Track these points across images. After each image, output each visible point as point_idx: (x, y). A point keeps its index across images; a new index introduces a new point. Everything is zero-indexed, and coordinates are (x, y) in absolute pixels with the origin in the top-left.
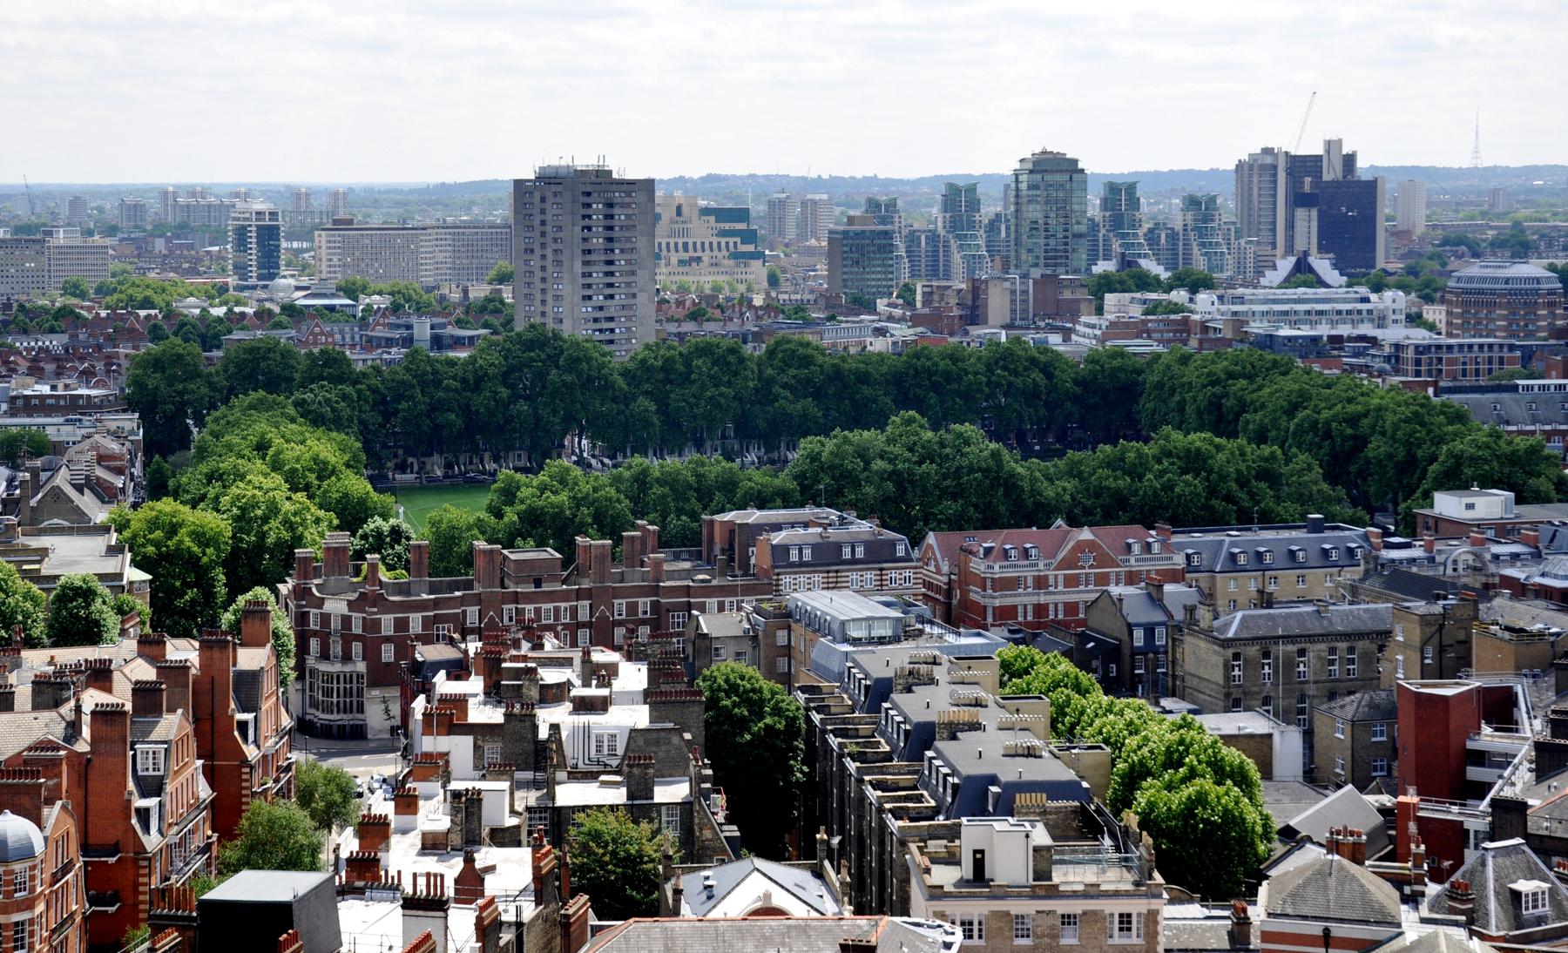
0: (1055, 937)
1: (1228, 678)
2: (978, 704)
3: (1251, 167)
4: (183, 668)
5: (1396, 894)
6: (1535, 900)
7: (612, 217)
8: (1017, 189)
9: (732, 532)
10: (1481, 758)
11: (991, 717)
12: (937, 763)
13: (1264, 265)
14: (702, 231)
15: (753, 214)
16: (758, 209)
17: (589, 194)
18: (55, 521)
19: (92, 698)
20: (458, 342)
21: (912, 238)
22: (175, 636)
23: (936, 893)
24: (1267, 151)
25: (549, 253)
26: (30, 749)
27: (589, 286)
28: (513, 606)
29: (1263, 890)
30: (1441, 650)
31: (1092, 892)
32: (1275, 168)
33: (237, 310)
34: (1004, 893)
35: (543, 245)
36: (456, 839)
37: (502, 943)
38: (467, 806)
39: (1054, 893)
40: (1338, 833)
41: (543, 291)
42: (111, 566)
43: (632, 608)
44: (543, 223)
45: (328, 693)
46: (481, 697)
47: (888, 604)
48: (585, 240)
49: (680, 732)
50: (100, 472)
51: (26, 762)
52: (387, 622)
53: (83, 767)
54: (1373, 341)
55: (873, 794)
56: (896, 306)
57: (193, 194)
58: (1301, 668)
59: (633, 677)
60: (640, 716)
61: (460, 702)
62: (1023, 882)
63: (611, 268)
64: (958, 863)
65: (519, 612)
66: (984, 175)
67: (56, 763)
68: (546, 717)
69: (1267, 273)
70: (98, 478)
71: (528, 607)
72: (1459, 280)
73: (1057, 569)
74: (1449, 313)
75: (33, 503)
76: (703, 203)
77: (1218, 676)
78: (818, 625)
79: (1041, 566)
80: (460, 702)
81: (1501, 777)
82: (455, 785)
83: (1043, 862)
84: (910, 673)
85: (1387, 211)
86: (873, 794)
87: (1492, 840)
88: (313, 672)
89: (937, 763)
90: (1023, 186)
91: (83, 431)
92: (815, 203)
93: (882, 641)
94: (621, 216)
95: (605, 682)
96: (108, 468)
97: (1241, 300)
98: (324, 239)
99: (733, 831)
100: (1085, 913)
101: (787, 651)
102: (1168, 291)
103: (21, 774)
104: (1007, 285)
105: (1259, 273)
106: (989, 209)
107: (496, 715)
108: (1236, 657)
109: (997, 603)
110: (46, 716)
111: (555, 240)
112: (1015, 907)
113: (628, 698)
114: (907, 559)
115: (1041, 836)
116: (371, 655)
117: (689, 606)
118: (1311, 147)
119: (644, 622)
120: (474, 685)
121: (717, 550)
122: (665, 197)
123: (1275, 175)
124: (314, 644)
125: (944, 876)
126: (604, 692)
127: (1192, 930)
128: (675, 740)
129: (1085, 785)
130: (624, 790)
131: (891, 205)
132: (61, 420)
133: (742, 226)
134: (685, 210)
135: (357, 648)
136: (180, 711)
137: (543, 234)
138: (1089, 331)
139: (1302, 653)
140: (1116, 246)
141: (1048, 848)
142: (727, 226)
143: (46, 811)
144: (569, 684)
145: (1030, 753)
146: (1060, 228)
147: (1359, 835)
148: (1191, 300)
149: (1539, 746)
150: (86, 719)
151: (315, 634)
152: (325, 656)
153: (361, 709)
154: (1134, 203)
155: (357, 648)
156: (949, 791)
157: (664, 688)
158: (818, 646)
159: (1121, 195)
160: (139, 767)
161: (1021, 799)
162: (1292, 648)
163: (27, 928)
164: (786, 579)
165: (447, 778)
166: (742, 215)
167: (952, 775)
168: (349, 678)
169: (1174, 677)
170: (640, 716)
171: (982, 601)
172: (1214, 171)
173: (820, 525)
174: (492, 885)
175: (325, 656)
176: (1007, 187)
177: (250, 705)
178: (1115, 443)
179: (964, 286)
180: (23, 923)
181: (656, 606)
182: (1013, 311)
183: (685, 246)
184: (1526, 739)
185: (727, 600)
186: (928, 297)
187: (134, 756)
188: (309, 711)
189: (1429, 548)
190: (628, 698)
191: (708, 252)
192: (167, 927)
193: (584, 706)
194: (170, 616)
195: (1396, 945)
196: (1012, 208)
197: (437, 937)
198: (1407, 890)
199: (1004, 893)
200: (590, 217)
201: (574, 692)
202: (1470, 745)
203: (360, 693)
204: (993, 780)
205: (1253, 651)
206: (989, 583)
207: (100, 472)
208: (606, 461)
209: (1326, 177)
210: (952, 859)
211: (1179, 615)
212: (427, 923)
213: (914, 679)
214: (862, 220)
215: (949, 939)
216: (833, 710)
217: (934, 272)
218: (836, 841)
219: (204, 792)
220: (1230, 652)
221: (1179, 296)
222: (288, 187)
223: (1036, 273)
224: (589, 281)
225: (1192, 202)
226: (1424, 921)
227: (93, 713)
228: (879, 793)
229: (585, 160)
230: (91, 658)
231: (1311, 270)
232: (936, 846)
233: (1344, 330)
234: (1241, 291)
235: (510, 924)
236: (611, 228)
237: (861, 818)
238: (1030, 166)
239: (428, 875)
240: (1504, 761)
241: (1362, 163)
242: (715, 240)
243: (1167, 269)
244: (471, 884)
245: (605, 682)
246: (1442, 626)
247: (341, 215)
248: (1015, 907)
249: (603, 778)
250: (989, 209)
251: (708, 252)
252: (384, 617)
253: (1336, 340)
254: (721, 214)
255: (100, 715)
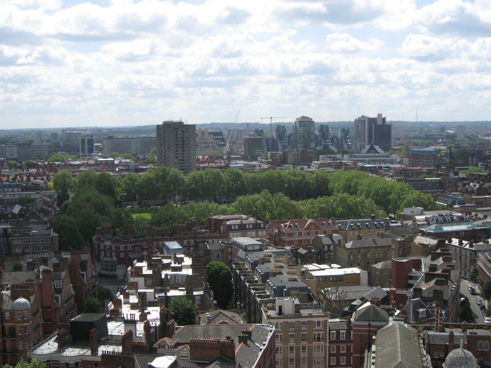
0: (301, 328)
1: (349, 258)
2: (281, 267)
3: (359, 121)
4: (66, 259)
5: (387, 314)
6: (422, 313)
8: (296, 126)
9: (216, 222)
10: (411, 278)
11: (285, 271)
12: (270, 283)
13: (363, 147)
14: (210, 139)
15: (224, 134)
16: (225, 133)
17: (177, 129)
18: (33, 220)
19: (42, 268)
20: (142, 170)
21: (267, 140)
22: (64, 251)
23: (269, 317)
24: (363, 117)
25: (166, 145)
26: (26, 281)
27: (177, 154)
28: (156, 242)
29: (354, 314)
30: (404, 250)
31: (310, 316)
32: (365, 121)
34: (286, 317)
35: (165, 143)
36: (140, 305)
37: (151, 332)
38: (142, 296)
39: (300, 316)
40: (374, 299)
41: (165, 156)
42: (47, 232)
43: (189, 242)
44: (165, 137)
45: (106, 266)
46: (146, 268)
47: (258, 241)
48: (176, 141)
49: (201, 276)
50: (45, 207)
51: (25, 284)
52: (122, 247)
53: (41, 286)
54: (390, 168)
55: (253, 292)
56: (263, 159)
57: (71, 130)
58: (368, 255)
59: (188, 261)
60: (189, 272)
61: (141, 268)
62: (292, 313)
63: (184, 152)
64: (275, 310)
65: (158, 244)
66: (287, 123)
67: (33, 285)
68: (164, 273)
69: (363, 149)
70: (44, 208)
71: (160, 242)
72: (412, 151)
73: (304, 230)
74: (409, 160)
75: (27, 215)
76: (210, 131)
77: (347, 258)
78: (239, 246)
79: (300, 229)
80: (141, 268)
81: (416, 282)
82: (140, 291)
83: (297, 308)
84: (263, 259)
85: (394, 133)
86: (253, 292)
87: (413, 298)
88: (102, 260)
89: (270, 283)
90: (297, 126)
91: (41, 195)
92: (241, 130)
93: (257, 251)
94: (186, 134)
95: (180, 263)
96: (47, 206)
97: (355, 157)
98: (105, 142)
99: (215, 302)
100: (308, 321)
101: (231, 253)
102: (336, 154)
103: (24, 287)
104: (293, 153)
105: (361, 150)
106: (288, 132)
107: (150, 272)
108: (351, 253)
109: (288, 240)
110: (30, 273)
111: (168, 142)
112: (290, 320)
113: (187, 267)
114: (264, 228)
115: (297, 302)
116: (118, 256)
117: (204, 242)
118: (374, 115)
119: (192, 246)
120: (144, 264)
121: (212, 225)
122: (199, 129)
123: (365, 123)
124: (102, 253)
125: (272, 313)
126: (180, 265)
127: (336, 325)
128: (199, 278)
129: (309, 288)
130: (185, 292)
131: (262, 131)
132: (35, 193)
133: (220, 137)
134: (205, 133)
135: (114, 254)
136: (65, 271)
137: (165, 140)
138: (315, 165)
139: (368, 251)
140: (323, 143)
141: (299, 305)
142: (216, 137)
143: (31, 297)
144: (170, 263)
145: (295, 280)
146: (308, 137)
147: (379, 299)
148: (343, 157)
149: (426, 274)
150: (41, 273)
151: (102, 250)
152: (105, 256)
153: (115, 270)
154: (327, 130)
155: (114, 254)
156: (273, 290)
157: (196, 264)
158: (239, 252)
159: (324, 128)
160: (55, 285)
161: (292, 292)
162: (366, 250)
163: (28, 327)
164: (231, 234)
165: (137, 289)
166: (221, 134)
167: (274, 286)
168: (112, 262)
169: (335, 258)
170: (189, 272)
171: (285, 239)
172: (349, 122)
173: (240, 219)
174: (149, 317)
175: (105, 256)
176: (293, 126)
177: (84, 269)
179: (281, 153)
180: (27, 326)
181: (195, 242)
182: (295, 160)
183: (205, 143)
184: (423, 272)
185: (215, 240)
186: (272, 157)
187: (54, 283)
188: (102, 271)
189: (402, 223)
190: (187, 267)
191: (211, 144)
192: (62, 328)
193: (174, 269)
194: (63, 246)
195: (386, 327)
196: (295, 132)
197: (133, 331)
198: (390, 312)
199: (286, 317)
200: (177, 135)
201: (172, 265)
202: (410, 274)
203: (115, 266)
204: (285, 287)
205: (356, 251)
206: (286, 234)
207: (45, 207)
208: (183, 202)
209: (378, 123)
210: (273, 309)
211: (336, 242)
212: (131, 328)
213: (265, 260)
214: (254, 135)
215: (271, 329)
216: (243, 269)
217: (273, 149)
218: (242, 305)
219: (73, 292)
220: (350, 252)
221: (339, 156)
222: (96, 128)
223: (301, 149)
225: (343, 130)
226: (394, 320)
227: (43, 272)
228: (254, 291)
229: (176, 119)
230: (42, 257)
231: (374, 149)
232: (269, 305)
233: (383, 165)
234: (356, 154)
235: (153, 327)
237: (249, 298)
238: (299, 120)
239: (131, 315)
240: (416, 278)
241: (388, 120)
242: (213, 141)
243: (336, 149)
244: (143, 317)
245: (180, 263)
246: (404, 244)
247: (110, 135)
248: (290, 320)
249: (179, 288)
250: (288, 132)
251: (211, 144)
252: (121, 246)
253: (380, 168)
254: (215, 134)
255: (45, 272)
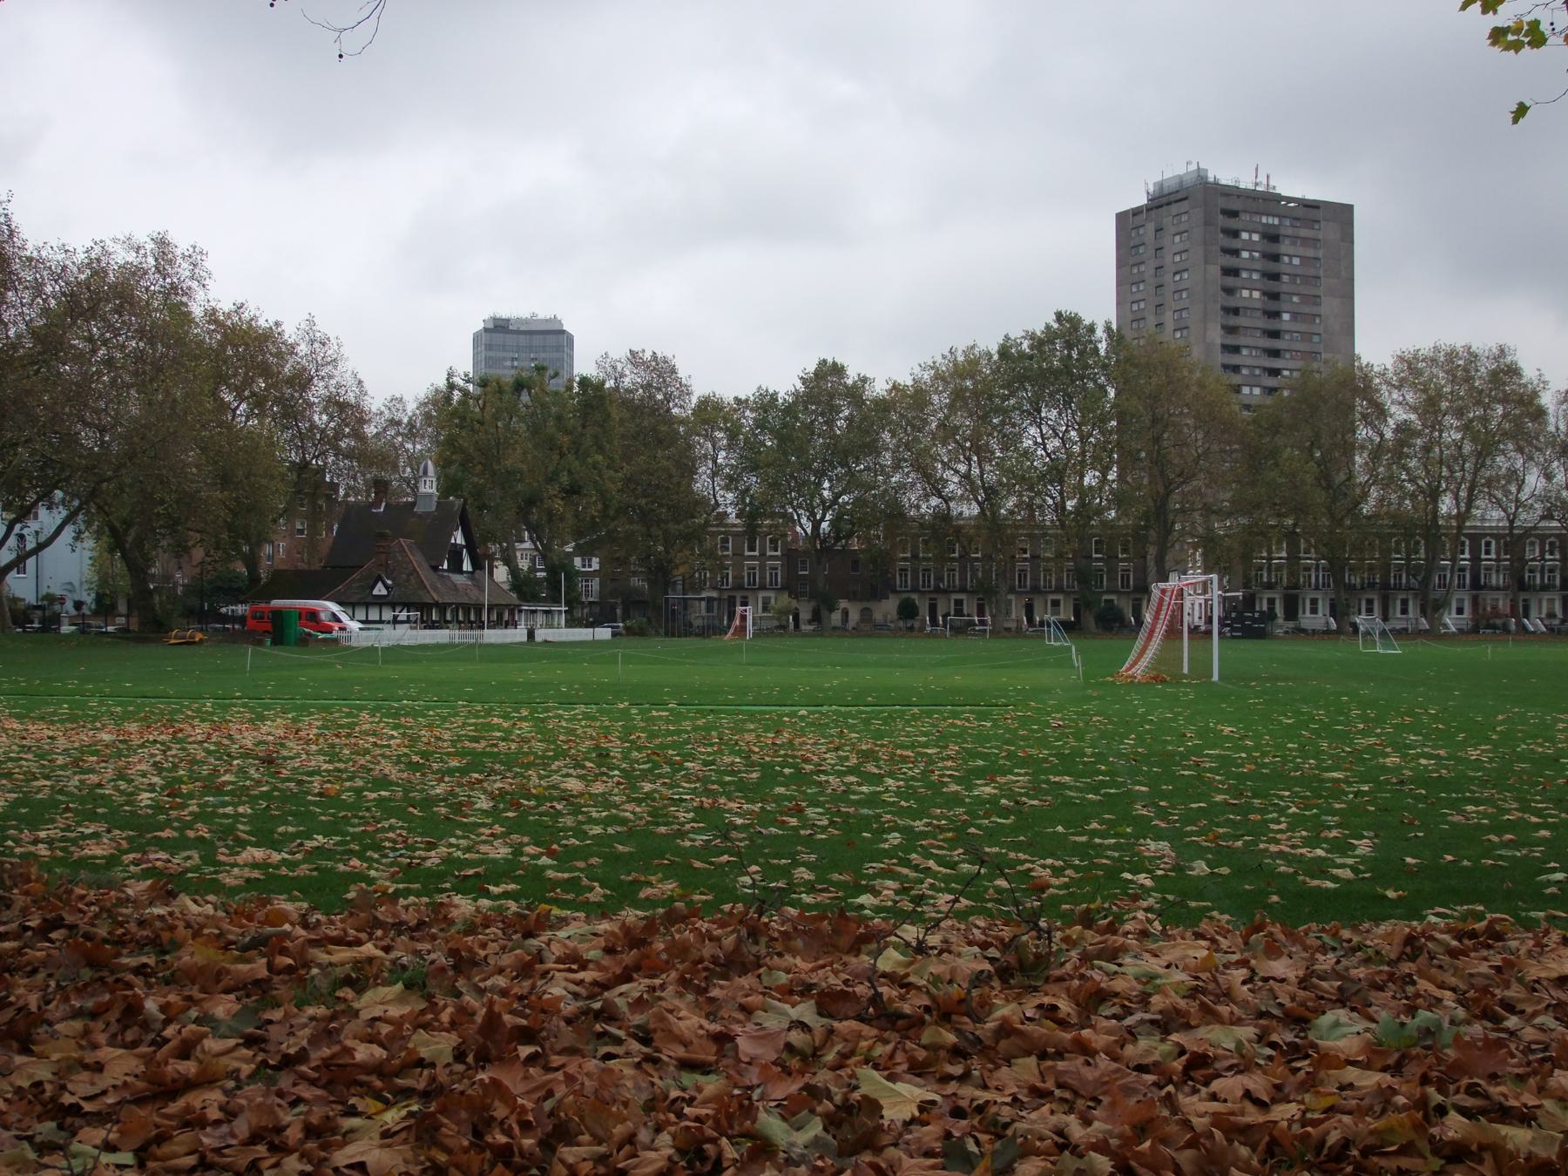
7: (1276, 258)
17: (1234, 214)
33: (576, 390)
178: (624, 926)
224: (1234, 360)
236: (1275, 277)
